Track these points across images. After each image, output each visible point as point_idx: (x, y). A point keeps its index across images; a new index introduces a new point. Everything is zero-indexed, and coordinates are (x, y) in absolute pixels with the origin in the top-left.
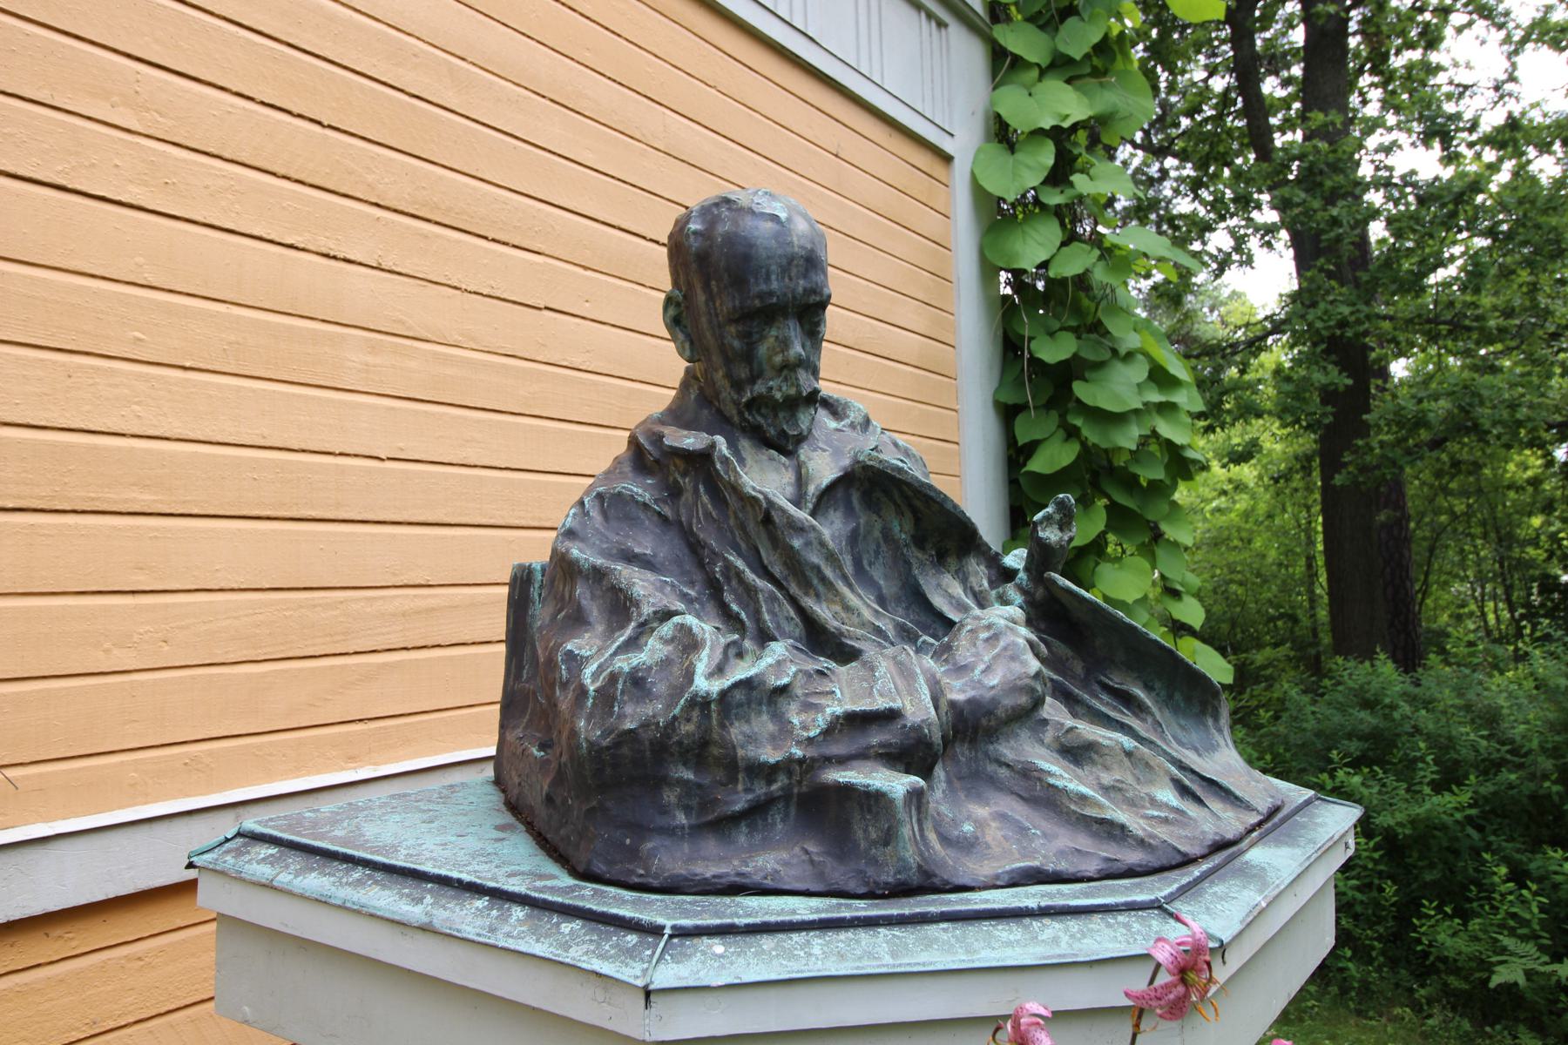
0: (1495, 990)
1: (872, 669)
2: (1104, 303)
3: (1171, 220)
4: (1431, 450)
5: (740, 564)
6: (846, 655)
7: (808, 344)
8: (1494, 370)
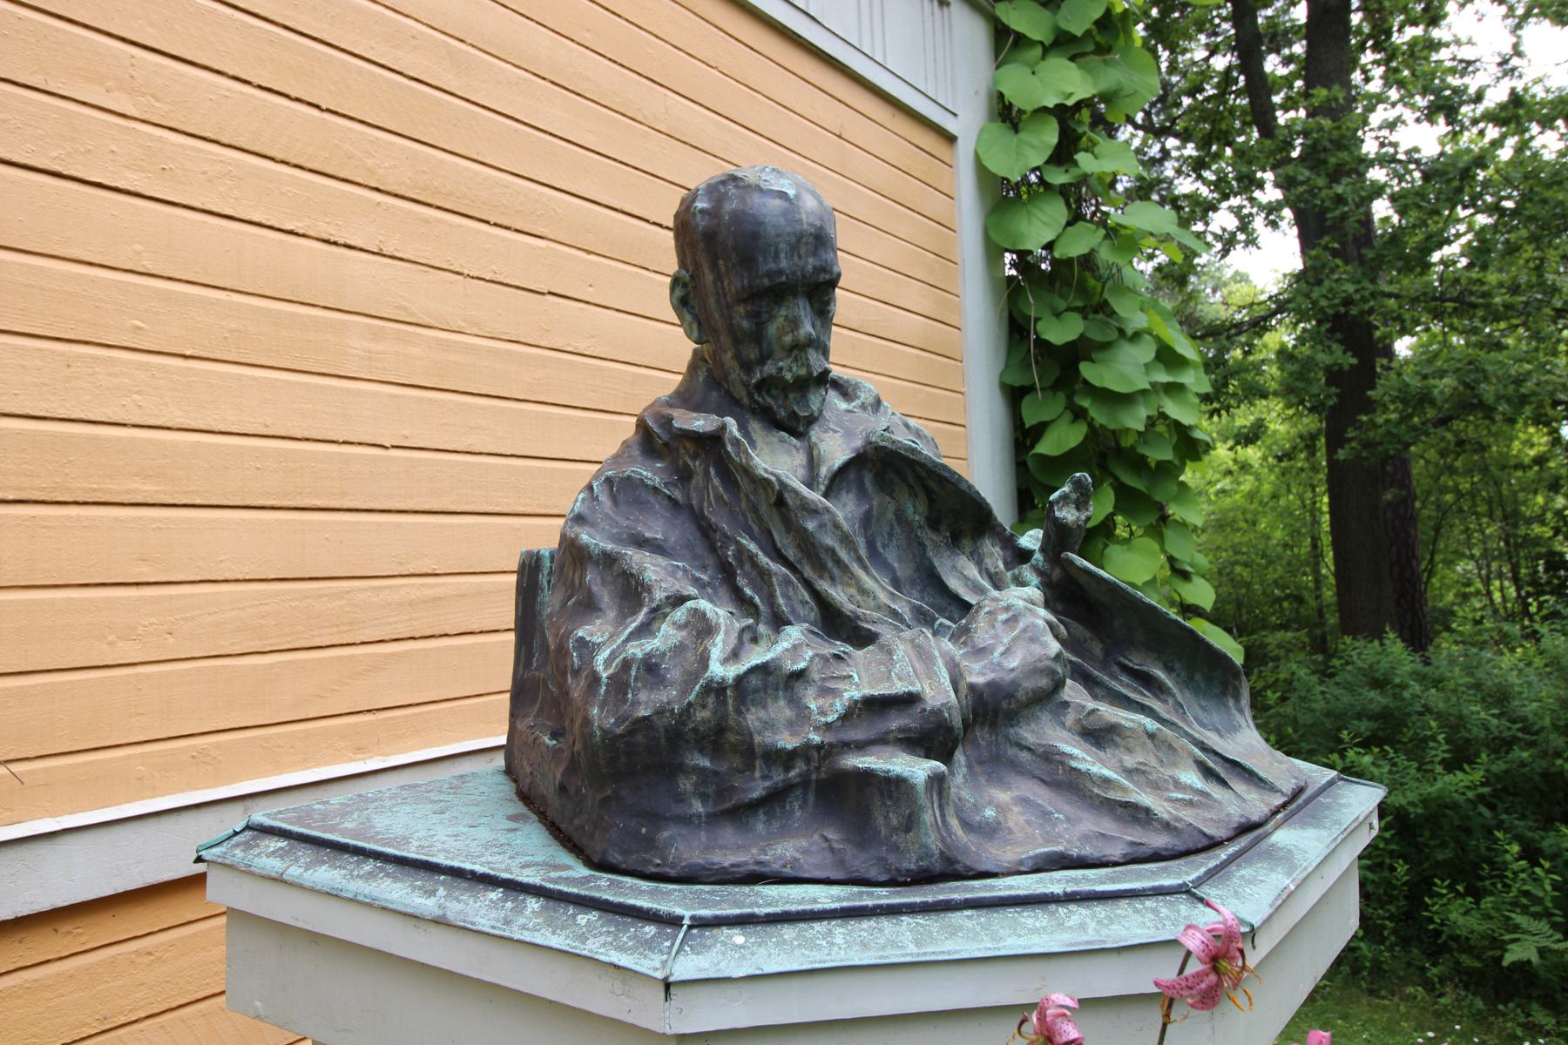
0: (1508, 968)
1: (890, 653)
2: (1110, 283)
3: (1175, 202)
4: (1435, 426)
5: (753, 547)
6: (862, 638)
7: (818, 323)
8: (1499, 346)
